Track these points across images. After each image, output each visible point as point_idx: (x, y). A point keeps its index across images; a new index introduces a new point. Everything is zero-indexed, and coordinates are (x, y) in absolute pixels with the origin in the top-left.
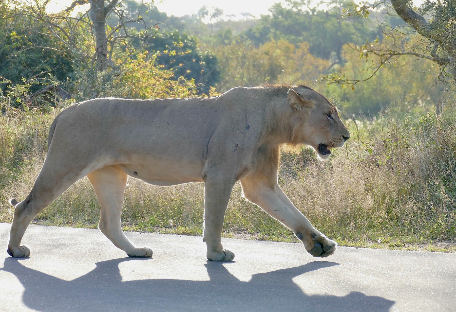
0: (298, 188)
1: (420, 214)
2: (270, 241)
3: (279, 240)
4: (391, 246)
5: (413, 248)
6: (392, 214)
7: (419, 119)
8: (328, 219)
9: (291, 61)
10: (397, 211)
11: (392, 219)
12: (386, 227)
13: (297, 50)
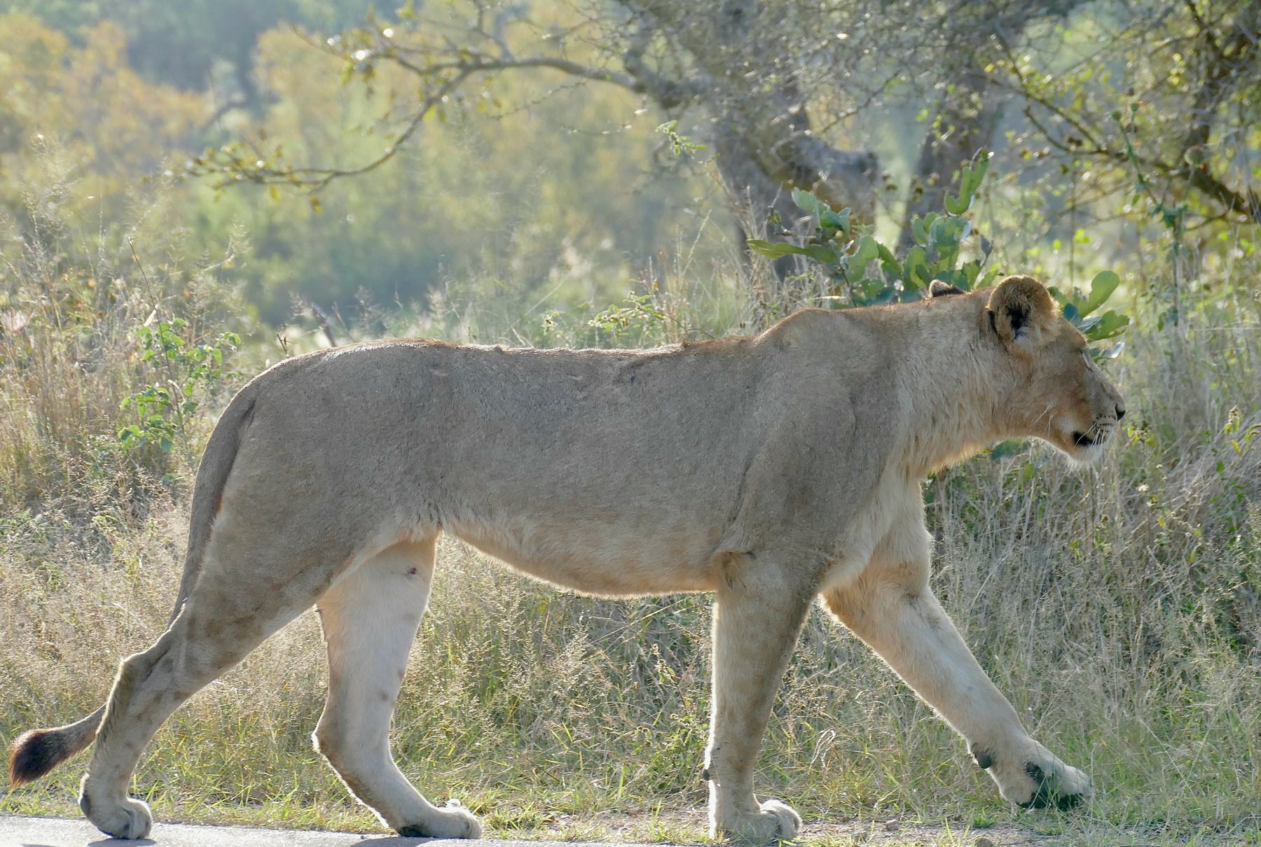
0: (117, 600)
1: (611, 695)
2: (11, 815)
3: (48, 810)
4: (497, 824)
5: (586, 831)
6: (502, 699)
7: (597, 318)
8: (244, 720)
9: (55, 98)
10: (521, 686)
11: (498, 718)
12: (473, 752)
13: (76, 53)
